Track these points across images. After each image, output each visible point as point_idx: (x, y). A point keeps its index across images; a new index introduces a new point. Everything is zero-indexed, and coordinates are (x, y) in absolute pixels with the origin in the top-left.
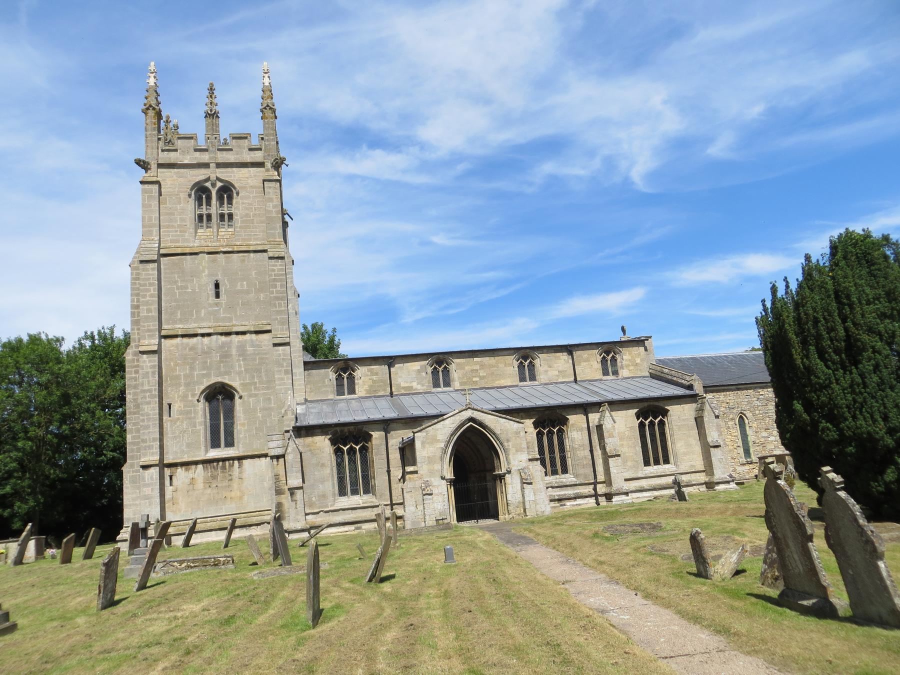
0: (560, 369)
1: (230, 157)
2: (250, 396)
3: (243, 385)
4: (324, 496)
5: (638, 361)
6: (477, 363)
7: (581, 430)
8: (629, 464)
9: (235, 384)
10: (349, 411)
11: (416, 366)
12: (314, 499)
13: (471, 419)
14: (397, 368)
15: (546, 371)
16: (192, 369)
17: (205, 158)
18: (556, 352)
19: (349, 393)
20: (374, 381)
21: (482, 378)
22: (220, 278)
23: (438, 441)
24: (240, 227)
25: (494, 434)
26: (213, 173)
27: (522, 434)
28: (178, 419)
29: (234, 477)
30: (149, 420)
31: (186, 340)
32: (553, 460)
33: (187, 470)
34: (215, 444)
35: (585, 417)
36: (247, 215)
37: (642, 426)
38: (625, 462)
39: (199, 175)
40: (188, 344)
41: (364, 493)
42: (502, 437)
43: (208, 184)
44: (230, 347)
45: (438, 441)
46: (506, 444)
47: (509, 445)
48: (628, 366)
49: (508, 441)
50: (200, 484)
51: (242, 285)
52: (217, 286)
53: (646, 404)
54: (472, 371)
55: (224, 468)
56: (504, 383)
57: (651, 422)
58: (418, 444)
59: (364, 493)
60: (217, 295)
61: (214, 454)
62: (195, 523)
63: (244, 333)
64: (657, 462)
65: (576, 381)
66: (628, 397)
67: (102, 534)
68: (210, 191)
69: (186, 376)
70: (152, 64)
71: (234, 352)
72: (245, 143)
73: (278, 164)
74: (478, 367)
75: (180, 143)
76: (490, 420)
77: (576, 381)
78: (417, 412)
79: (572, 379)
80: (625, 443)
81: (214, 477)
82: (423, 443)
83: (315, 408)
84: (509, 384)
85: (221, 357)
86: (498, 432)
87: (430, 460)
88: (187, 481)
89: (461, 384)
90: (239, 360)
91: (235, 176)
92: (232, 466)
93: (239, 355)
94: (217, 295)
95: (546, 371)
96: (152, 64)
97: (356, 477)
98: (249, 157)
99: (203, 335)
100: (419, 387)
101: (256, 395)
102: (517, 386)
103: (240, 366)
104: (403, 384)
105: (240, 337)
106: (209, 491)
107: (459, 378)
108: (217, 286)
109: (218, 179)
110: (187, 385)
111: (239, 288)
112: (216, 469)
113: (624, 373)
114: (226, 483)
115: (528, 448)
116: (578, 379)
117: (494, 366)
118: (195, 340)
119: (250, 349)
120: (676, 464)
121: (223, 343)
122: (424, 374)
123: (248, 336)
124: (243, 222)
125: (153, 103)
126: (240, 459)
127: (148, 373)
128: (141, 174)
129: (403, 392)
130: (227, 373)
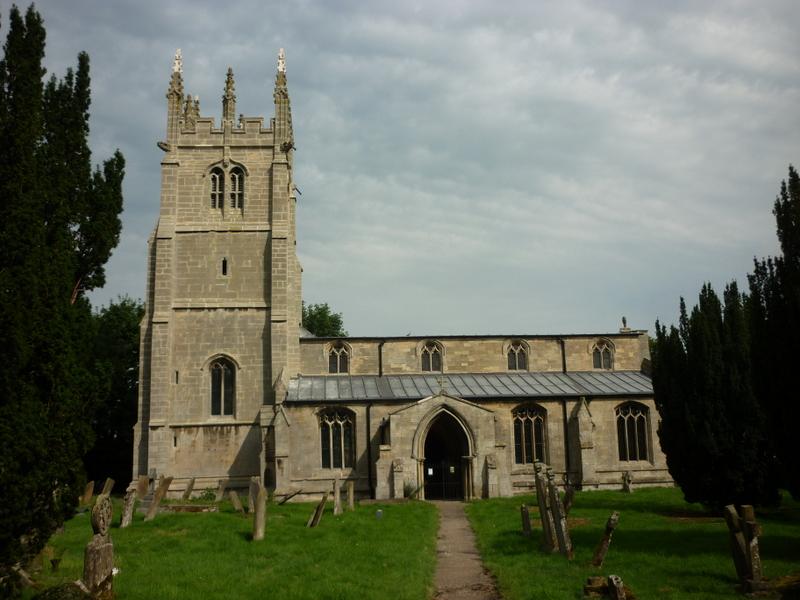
0: (550, 359)
1: (245, 141)
2: (248, 368)
3: (243, 358)
4: (308, 467)
5: (631, 355)
6: (467, 348)
7: (558, 421)
8: (604, 457)
9: (236, 357)
10: (521, 385)
11: (406, 347)
12: (299, 469)
13: (445, 406)
14: (387, 345)
15: (536, 360)
16: (198, 340)
17: (220, 141)
18: (264, 350)
19: (520, 368)
20: (365, 361)
21: (470, 364)
22: (227, 255)
23: (412, 424)
24: (249, 207)
25: (465, 421)
26: (230, 155)
27: (492, 422)
28: (184, 386)
29: (230, 443)
30: (158, 386)
31: (194, 313)
32: (529, 448)
33: (190, 433)
34: (216, 411)
35: (561, 406)
36: (256, 197)
37: (620, 421)
38: (599, 454)
39: (215, 157)
40: (195, 317)
41: (335, 467)
42: (472, 424)
43: (220, 166)
44: (232, 322)
45: (412, 424)
46: (475, 431)
47: (479, 432)
48: (620, 359)
49: (477, 428)
50: (200, 447)
51: (247, 263)
52: (225, 263)
53: (621, 402)
54: (462, 355)
55: (222, 433)
56: (495, 372)
57: (630, 418)
58: (393, 425)
59: (335, 467)
60: (225, 272)
61: (214, 420)
62: (193, 482)
63: (246, 309)
64: (633, 458)
65: (565, 371)
66: (608, 391)
67: (115, 485)
68: (223, 172)
69: (192, 347)
70: (282, 50)
71: (236, 326)
72: (257, 127)
73: (287, 148)
74: (467, 353)
75: (198, 127)
76: (461, 407)
77: (565, 371)
78: (399, 394)
79: (561, 370)
80: (601, 437)
81: (213, 441)
82: (397, 425)
83: (307, 384)
84: (497, 371)
85: (225, 330)
86: (468, 419)
87: (403, 441)
88: (189, 443)
89: (450, 368)
90: (240, 334)
91: (249, 159)
92: (229, 432)
93: (241, 330)
94: (225, 272)
95: (536, 360)
96: (282, 50)
97: (531, 446)
98: (259, 141)
99: (209, 309)
100: (408, 369)
101: (253, 368)
102: (589, 373)
103: (241, 339)
104: (393, 366)
105: (243, 313)
106: (207, 454)
107: (448, 362)
108: (225, 263)
109: (232, 162)
110: (193, 355)
111: (244, 266)
112: (214, 433)
113: (617, 366)
114: (222, 448)
115: (496, 434)
116: (568, 370)
117: (483, 353)
118: (202, 313)
119: (251, 324)
120: (652, 462)
121: (228, 318)
122: (413, 356)
123: (249, 313)
124: (252, 203)
125: (176, 88)
126: (237, 426)
127: (159, 342)
128: (162, 156)
129: (393, 373)
130: (230, 346)
